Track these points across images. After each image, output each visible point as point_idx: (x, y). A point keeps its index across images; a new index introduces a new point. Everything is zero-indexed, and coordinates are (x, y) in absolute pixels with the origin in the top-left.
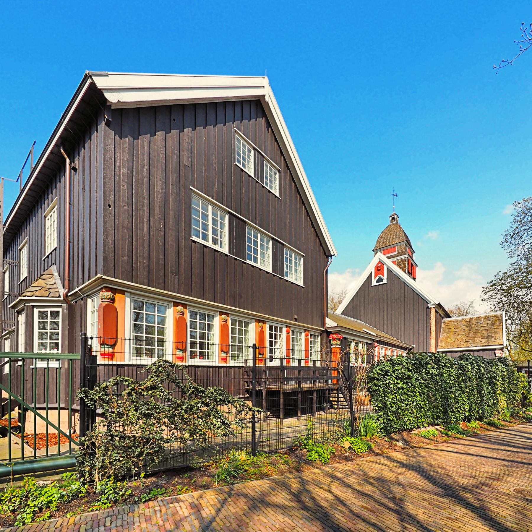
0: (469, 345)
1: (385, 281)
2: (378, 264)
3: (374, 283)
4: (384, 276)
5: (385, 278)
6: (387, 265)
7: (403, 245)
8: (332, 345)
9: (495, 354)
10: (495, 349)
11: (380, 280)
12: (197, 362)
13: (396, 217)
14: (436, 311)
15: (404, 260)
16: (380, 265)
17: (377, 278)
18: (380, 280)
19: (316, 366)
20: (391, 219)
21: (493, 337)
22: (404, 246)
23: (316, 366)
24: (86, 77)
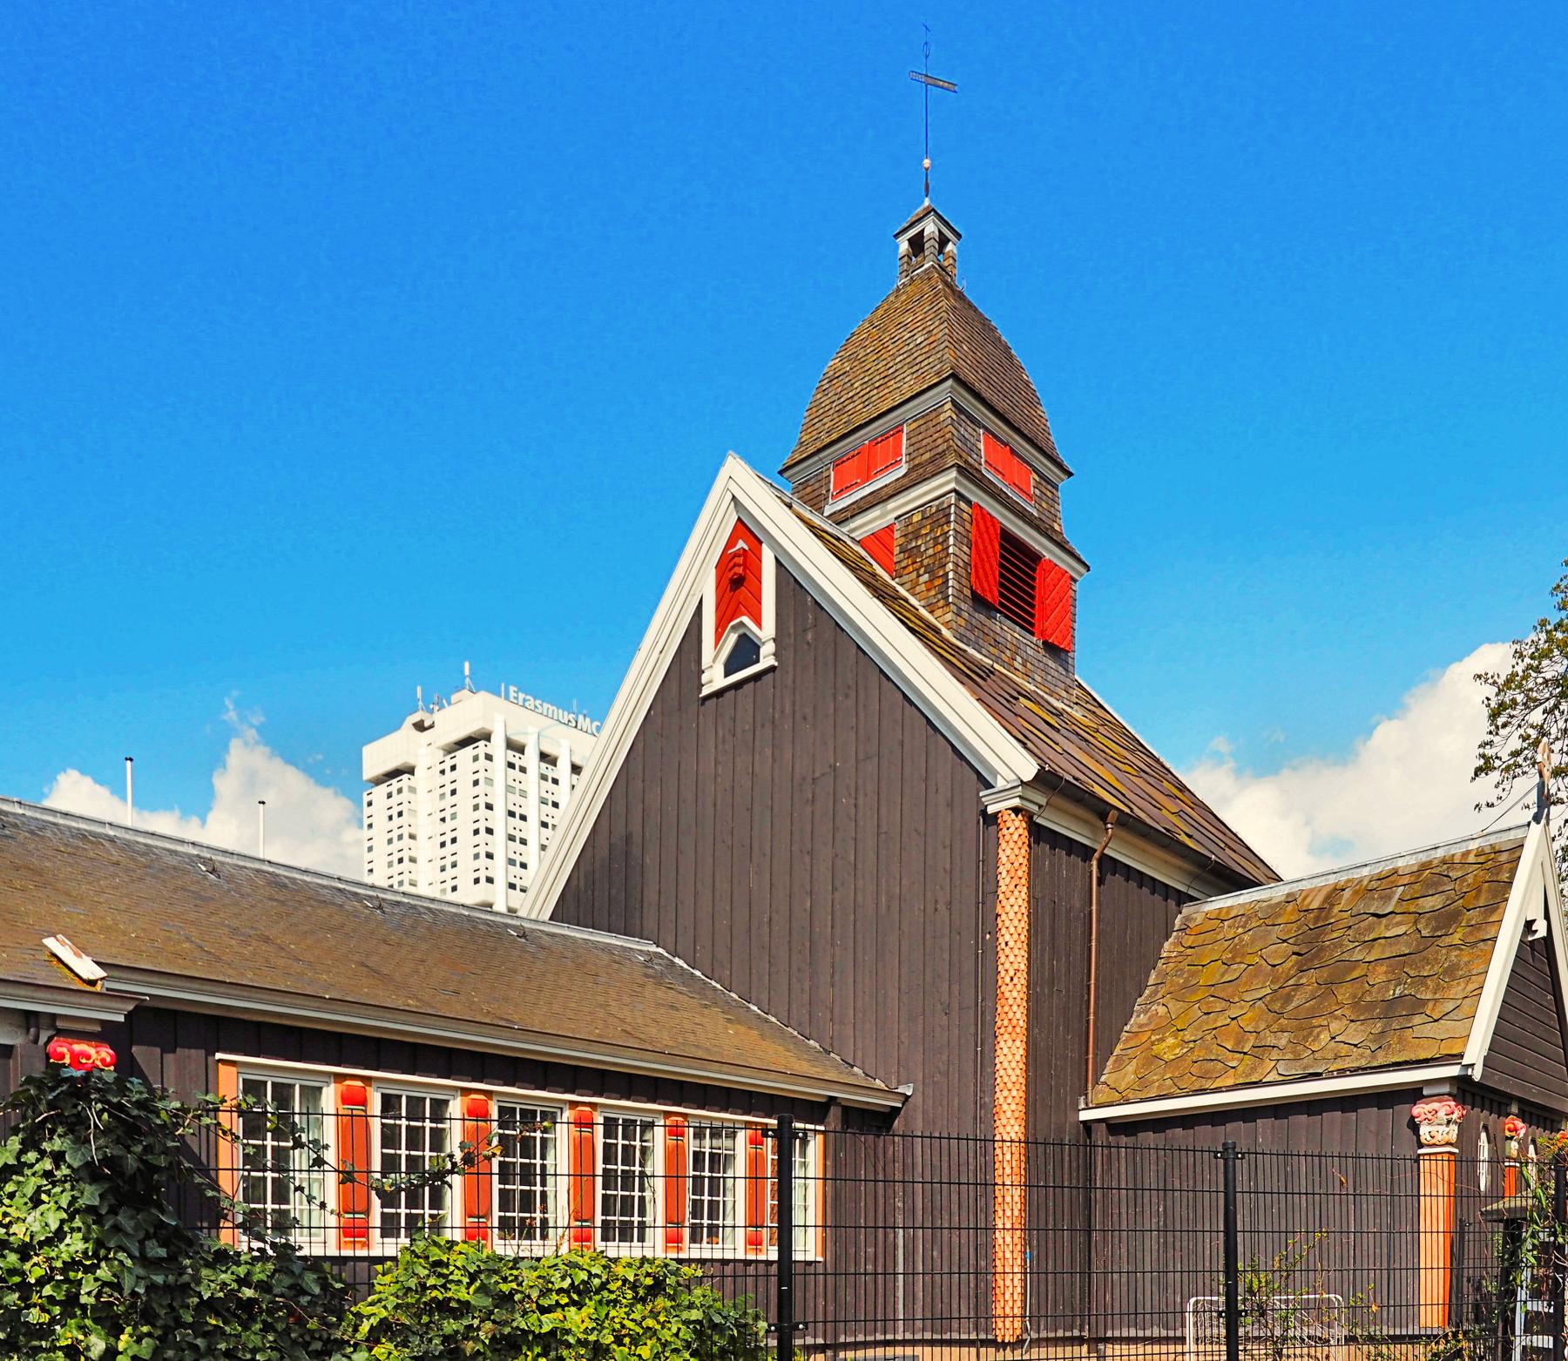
0: (1267, 1071)
1: (767, 659)
2: (731, 543)
3: (715, 678)
4: (759, 623)
5: (766, 631)
6: (775, 545)
7: (938, 409)
8: (1421, 1146)
9: (1414, 1127)
10: (1414, 1093)
11: (746, 651)
12: (704, 1251)
13: (930, 228)
14: (1037, 833)
15: (937, 516)
16: (741, 544)
17: (731, 640)
18: (746, 651)
19: (798, 1256)
20: (904, 246)
21: (1418, 1006)
22: (948, 412)
23: (798, 1256)
24: (958, 236)
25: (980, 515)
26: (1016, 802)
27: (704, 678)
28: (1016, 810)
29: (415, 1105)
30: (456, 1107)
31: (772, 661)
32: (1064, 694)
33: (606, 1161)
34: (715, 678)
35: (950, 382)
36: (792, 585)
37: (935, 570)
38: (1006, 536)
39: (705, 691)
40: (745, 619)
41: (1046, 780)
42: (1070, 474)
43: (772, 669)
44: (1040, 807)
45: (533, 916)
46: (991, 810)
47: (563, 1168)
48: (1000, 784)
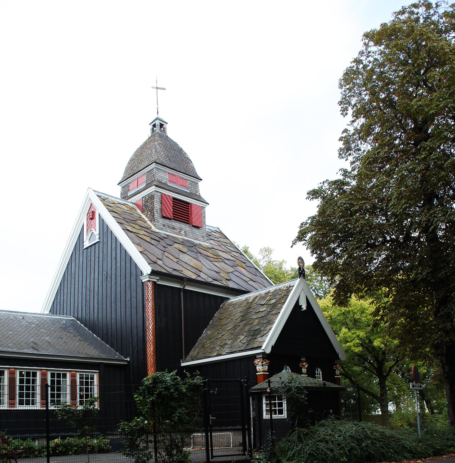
5: (97, 232)
15: (151, 197)
25: (162, 195)
26: (148, 279)
27: (84, 244)
28: (149, 281)
29: (28, 374)
30: (38, 374)
31: (98, 240)
32: (202, 239)
33: (80, 391)
34: (87, 244)
35: (154, 163)
36: (102, 222)
37: (152, 211)
38: (174, 199)
39: (84, 248)
40: (93, 229)
41: (153, 273)
42: (201, 180)
43: (98, 242)
44: (157, 280)
45: (42, 313)
46: (143, 281)
47: (6, 393)
48: (145, 274)
